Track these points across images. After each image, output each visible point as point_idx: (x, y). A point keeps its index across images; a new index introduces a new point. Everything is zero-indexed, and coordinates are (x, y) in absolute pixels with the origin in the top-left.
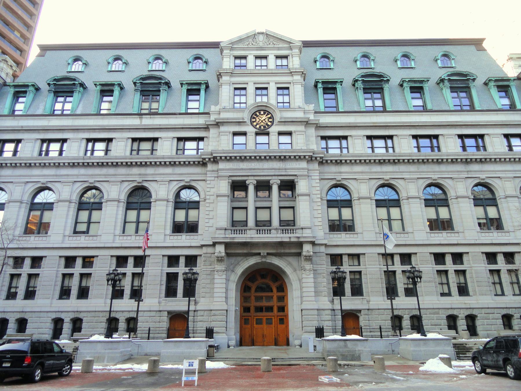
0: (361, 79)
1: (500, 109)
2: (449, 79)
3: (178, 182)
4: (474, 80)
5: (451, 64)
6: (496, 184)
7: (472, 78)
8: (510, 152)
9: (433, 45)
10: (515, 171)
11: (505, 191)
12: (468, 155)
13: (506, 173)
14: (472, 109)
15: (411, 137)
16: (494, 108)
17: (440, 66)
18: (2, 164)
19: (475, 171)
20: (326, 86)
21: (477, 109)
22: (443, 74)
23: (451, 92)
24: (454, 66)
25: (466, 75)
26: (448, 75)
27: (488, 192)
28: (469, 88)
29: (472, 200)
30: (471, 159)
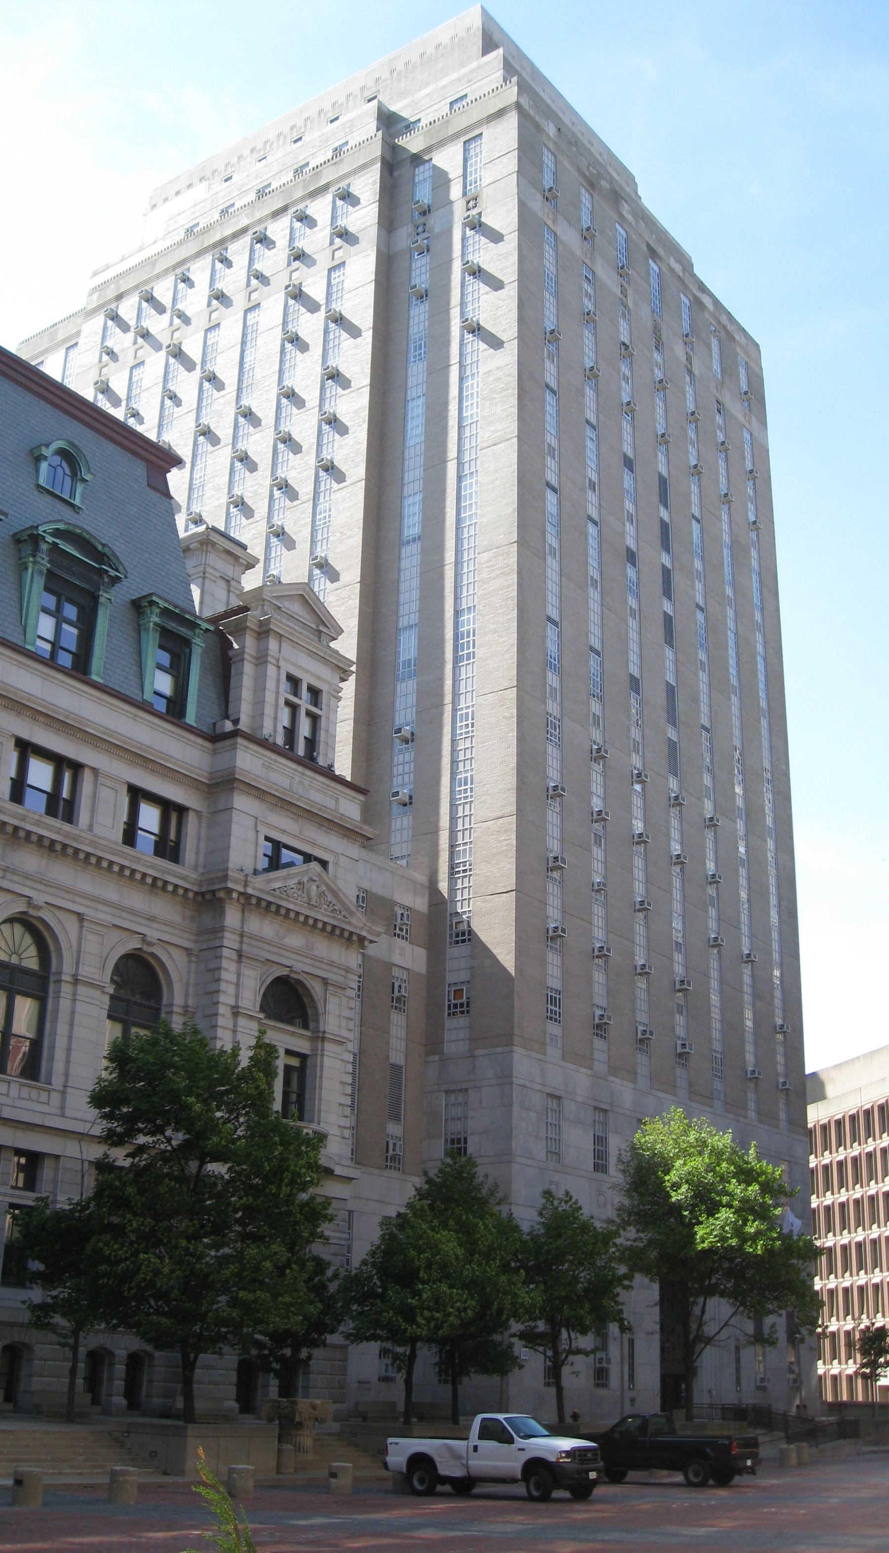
0: (50, 539)
1: (145, 702)
2: (55, 545)
3: (124, 934)
4: (116, 580)
5: (73, 494)
6: (66, 930)
7: (113, 573)
8: (127, 849)
9: (76, 418)
10: (123, 908)
11: (78, 963)
12: (24, 818)
13: (100, 906)
14: (81, 667)
15: (13, 741)
16: (132, 692)
17: (42, 481)
18: (4, 823)
19: (25, 876)
20: (172, 625)
21: (94, 677)
22: (47, 518)
23: (47, 589)
24: (77, 502)
25: (101, 557)
26: (57, 533)
27: (32, 951)
28: (95, 599)
29: (107, 999)
30: (29, 833)
